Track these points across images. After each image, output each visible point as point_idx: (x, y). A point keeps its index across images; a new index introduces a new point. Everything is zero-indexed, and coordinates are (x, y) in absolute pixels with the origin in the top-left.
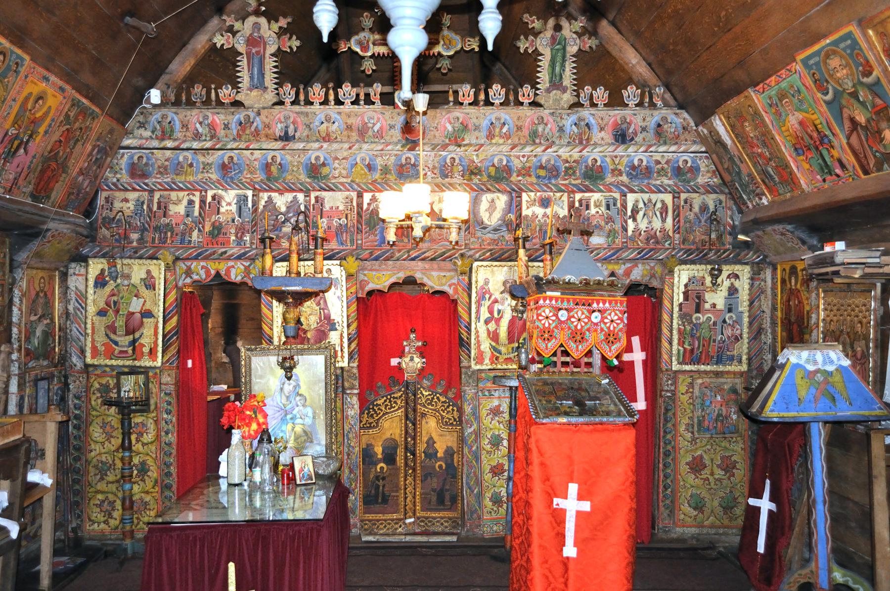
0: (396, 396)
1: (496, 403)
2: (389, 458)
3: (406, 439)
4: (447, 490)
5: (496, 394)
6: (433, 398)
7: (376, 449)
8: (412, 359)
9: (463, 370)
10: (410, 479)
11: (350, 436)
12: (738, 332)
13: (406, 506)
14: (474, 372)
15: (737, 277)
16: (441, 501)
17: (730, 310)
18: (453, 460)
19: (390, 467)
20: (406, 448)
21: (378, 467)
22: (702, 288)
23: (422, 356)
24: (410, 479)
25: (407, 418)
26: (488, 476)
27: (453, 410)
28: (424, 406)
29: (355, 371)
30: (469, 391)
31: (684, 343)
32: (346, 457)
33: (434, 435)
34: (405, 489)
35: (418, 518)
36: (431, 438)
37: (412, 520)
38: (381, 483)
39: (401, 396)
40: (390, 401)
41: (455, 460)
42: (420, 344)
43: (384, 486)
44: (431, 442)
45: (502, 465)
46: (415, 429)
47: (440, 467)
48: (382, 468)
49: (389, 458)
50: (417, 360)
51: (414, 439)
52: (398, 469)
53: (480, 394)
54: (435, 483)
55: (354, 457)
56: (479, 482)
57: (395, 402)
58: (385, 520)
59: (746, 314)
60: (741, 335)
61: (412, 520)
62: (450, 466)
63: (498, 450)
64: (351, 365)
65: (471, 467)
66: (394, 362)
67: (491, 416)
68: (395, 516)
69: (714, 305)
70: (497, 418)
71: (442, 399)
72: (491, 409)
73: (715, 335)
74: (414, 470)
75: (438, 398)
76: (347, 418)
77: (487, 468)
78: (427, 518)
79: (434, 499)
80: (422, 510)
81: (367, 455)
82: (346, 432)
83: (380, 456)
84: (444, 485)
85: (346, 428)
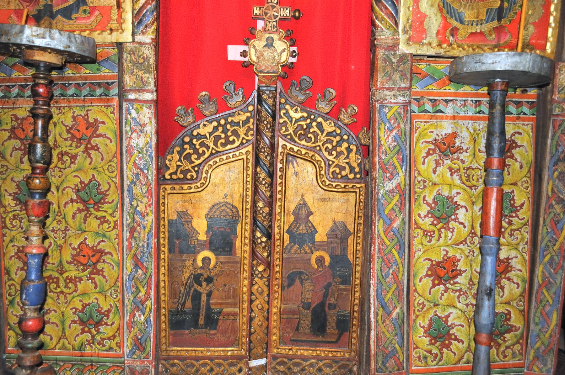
0: (236, 119)
1: (447, 128)
2: (222, 243)
3: (254, 203)
4: (332, 307)
5: (449, 110)
6: (309, 126)
7: (195, 223)
8: (270, 44)
9: (380, 53)
10: (260, 283)
11: (136, 190)
13: (250, 334)
14: (403, 57)
16: (319, 325)
18: (345, 249)
19: (222, 258)
20: (254, 222)
21: (200, 257)
23: (291, 39)
24: (260, 283)
25: (257, 161)
26: (423, 284)
27: (349, 150)
28: (292, 140)
29: (149, 53)
30: (389, 96)
32: (126, 235)
33: (309, 200)
34: (251, 302)
35: (275, 358)
36: (303, 204)
37: (263, 361)
38: (204, 288)
39: (247, 121)
40: (225, 131)
41: (350, 249)
42: (286, 12)
43: (209, 295)
44: (303, 212)
45: (454, 261)
46: (272, 185)
47: (320, 260)
48: (206, 260)
49: (222, 243)
50: (280, 45)
51: (270, 204)
52: (238, 263)
53: (415, 107)
54: (308, 292)
55: (143, 234)
56: (407, 294)
57: (235, 133)
58: (211, 359)
61: (263, 361)
62: (339, 260)
63: (448, 229)
64: (139, 38)
65: (387, 263)
66: (234, 53)
67: (435, 157)
68: (230, 351)
70: (448, 162)
71: (328, 127)
72: (436, 142)
74: (269, 265)
75: (319, 125)
76: (130, 152)
77: (421, 267)
78: (290, 358)
79: (307, 321)
80: (282, 341)
81: (178, 238)
82: (126, 183)
83: (203, 237)
84: (325, 296)
85: (128, 173)
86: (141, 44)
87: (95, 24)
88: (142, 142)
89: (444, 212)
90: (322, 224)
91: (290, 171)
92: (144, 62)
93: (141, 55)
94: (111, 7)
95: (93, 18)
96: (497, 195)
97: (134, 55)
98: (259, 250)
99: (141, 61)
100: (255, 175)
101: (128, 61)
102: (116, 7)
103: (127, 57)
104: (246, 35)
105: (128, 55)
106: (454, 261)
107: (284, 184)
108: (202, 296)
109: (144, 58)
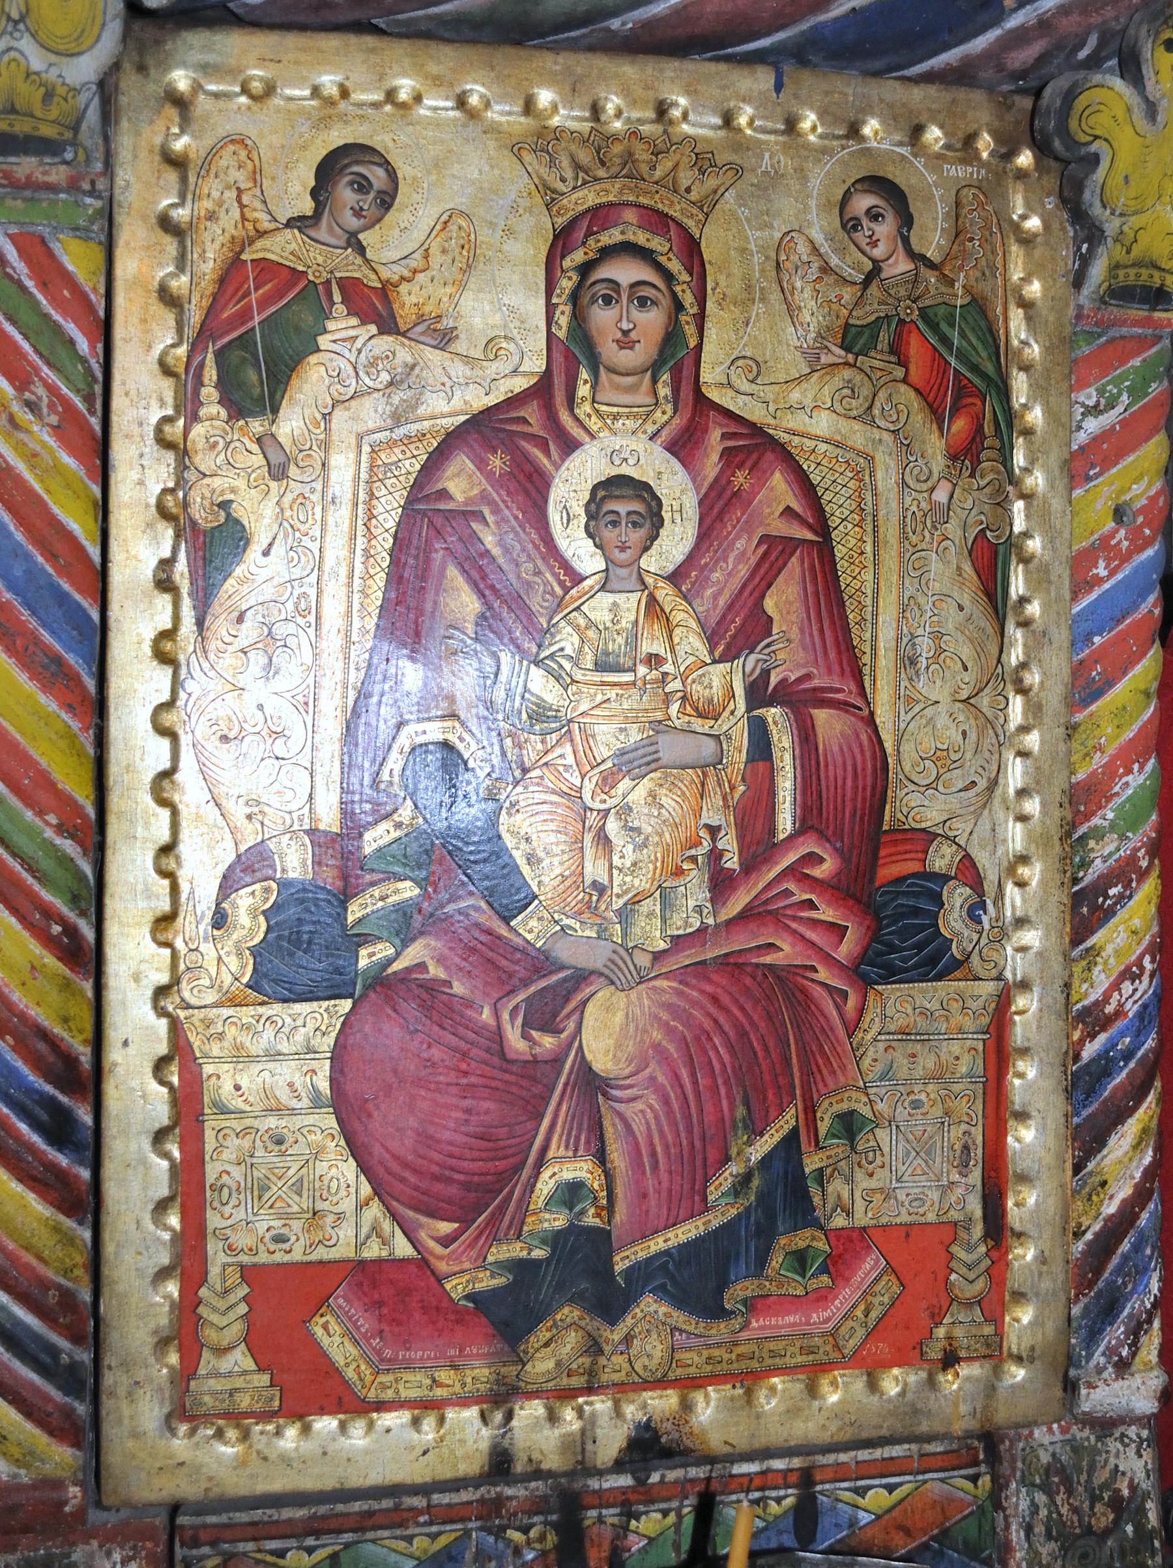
86: (1105, 1425)
87: (861, 1333)
92: (1116, 1522)
93: (1104, 1486)
94: (954, 1229)
95: (847, 1295)
96: (795, 36)
97: (1070, 1492)
99: (1103, 1518)
101: (1039, 1529)
102: (978, 1231)
103: (1034, 1508)
105: (1041, 1498)
108: (215, 378)
109: (1117, 1503)
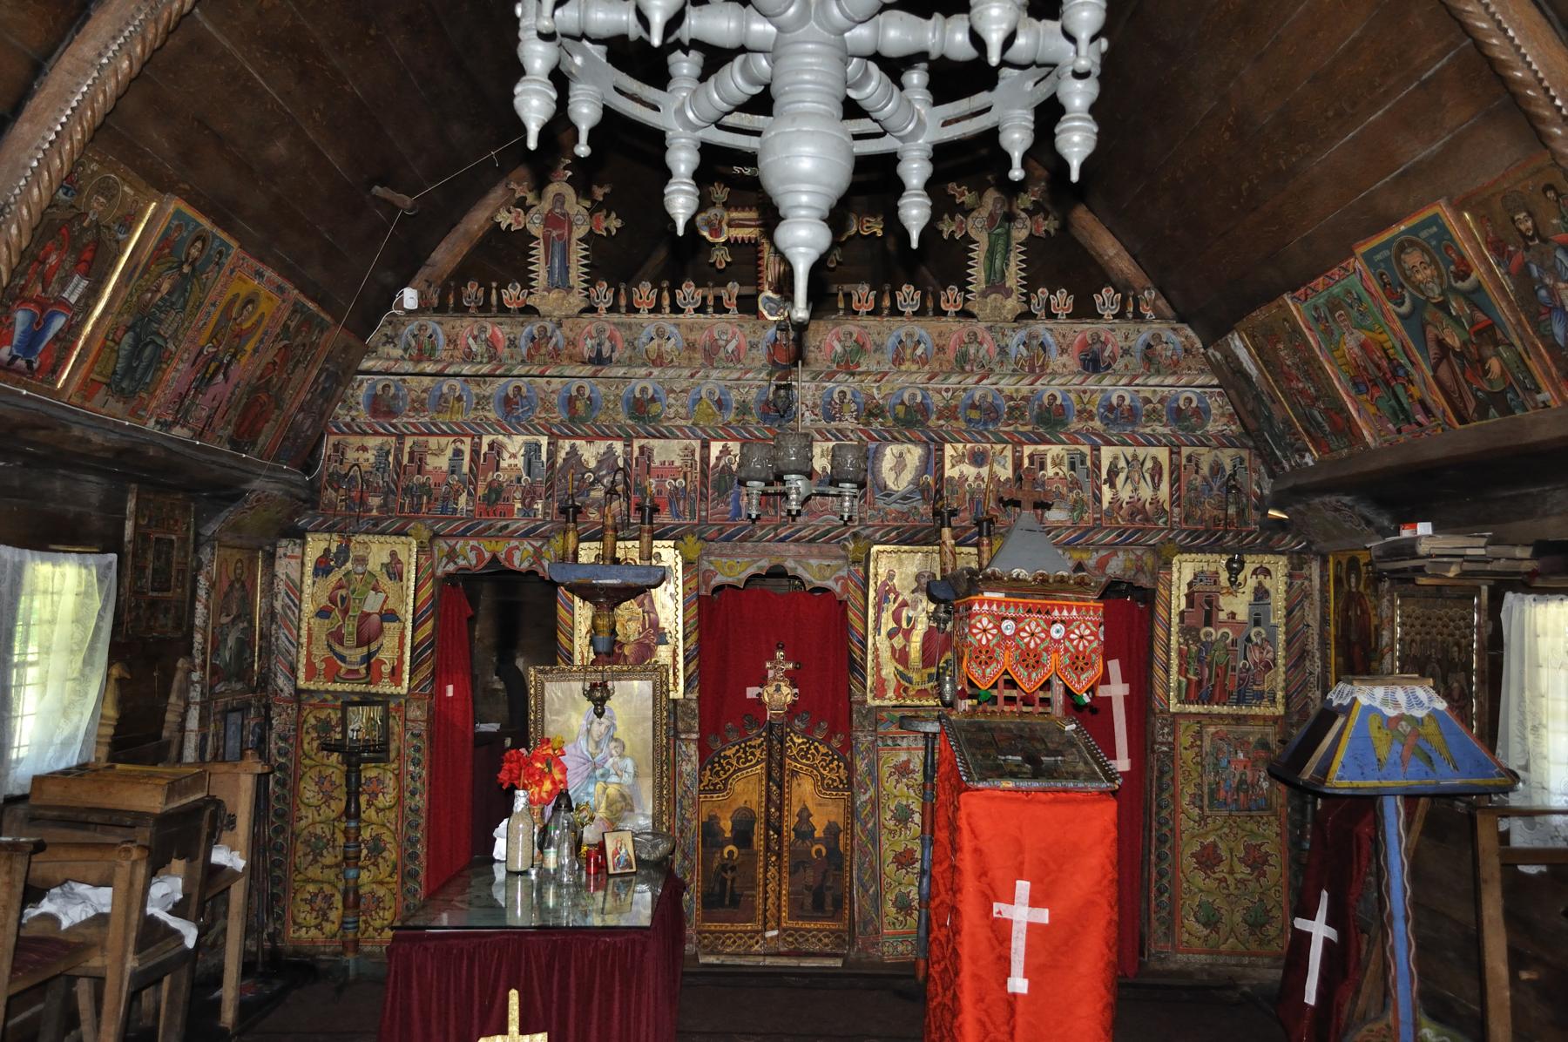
1: (903, 757)
2: (743, 836)
3: (767, 810)
5: (904, 744)
8: (778, 689)
9: (855, 707)
10: (772, 870)
11: (685, 803)
12: (1270, 655)
15: (1267, 572)
16: (818, 905)
17: (1257, 623)
20: (768, 821)
21: (726, 851)
22: (1214, 588)
23: (793, 685)
24: (772, 870)
25: (769, 777)
26: (890, 868)
29: (694, 705)
30: (863, 739)
31: (1187, 671)
33: (810, 805)
35: (785, 930)
36: (805, 809)
37: (775, 933)
38: (729, 875)
43: (733, 880)
45: (912, 852)
46: (781, 795)
47: (819, 852)
49: (743, 836)
50: (785, 690)
51: (780, 809)
52: (756, 854)
54: (809, 877)
55: (690, 835)
56: (877, 877)
57: (752, 754)
58: (735, 933)
59: (1282, 629)
60: (1274, 660)
61: (775, 933)
62: (833, 851)
66: (752, 692)
68: (749, 926)
69: (1233, 615)
71: (823, 750)
72: (895, 767)
73: (1235, 659)
74: (779, 855)
78: (797, 930)
79: (809, 901)
81: (710, 831)
83: (728, 835)
88: (689, 768)
89: (903, 817)
90: (819, 824)
91: (795, 783)
98: (772, 844)
100: (768, 787)
104: (762, 682)
106: (912, 852)
107: (790, 793)
